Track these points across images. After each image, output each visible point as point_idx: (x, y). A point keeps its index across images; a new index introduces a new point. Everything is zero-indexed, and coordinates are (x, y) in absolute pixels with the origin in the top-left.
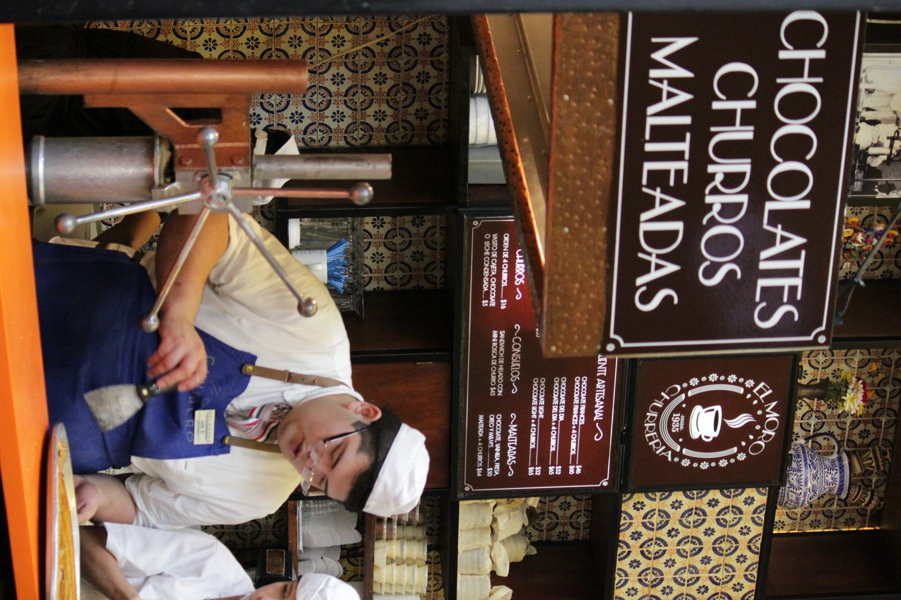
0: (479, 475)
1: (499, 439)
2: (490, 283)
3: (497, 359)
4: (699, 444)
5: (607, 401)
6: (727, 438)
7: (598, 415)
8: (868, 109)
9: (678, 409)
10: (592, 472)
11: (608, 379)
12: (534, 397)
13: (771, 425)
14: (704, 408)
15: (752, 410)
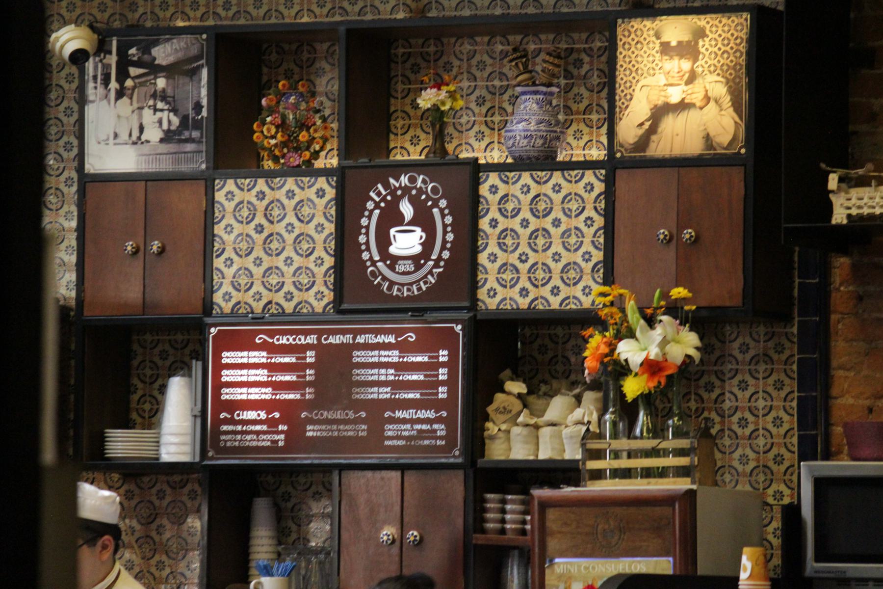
0: (444, 443)
1: (408, 426)
2: (263, 440)
3: (332, 431)
4: (428, 245)
5: (377, 332)
6: (423, 220)
7: (391, 339)
8: (130, 135)
9: (392, 268)
10: (447, 339)
11: (356, 333)
12: (370, 397)
13: (413, 180)
14: (391, 244)
15: (397, 200)
